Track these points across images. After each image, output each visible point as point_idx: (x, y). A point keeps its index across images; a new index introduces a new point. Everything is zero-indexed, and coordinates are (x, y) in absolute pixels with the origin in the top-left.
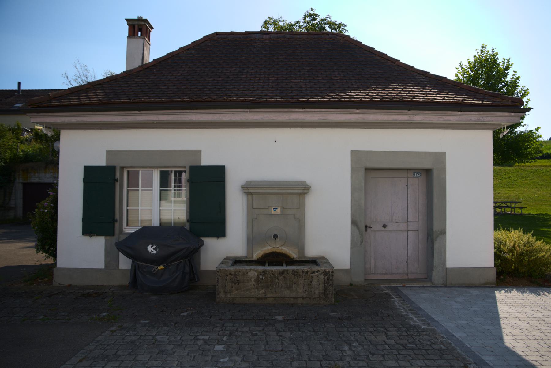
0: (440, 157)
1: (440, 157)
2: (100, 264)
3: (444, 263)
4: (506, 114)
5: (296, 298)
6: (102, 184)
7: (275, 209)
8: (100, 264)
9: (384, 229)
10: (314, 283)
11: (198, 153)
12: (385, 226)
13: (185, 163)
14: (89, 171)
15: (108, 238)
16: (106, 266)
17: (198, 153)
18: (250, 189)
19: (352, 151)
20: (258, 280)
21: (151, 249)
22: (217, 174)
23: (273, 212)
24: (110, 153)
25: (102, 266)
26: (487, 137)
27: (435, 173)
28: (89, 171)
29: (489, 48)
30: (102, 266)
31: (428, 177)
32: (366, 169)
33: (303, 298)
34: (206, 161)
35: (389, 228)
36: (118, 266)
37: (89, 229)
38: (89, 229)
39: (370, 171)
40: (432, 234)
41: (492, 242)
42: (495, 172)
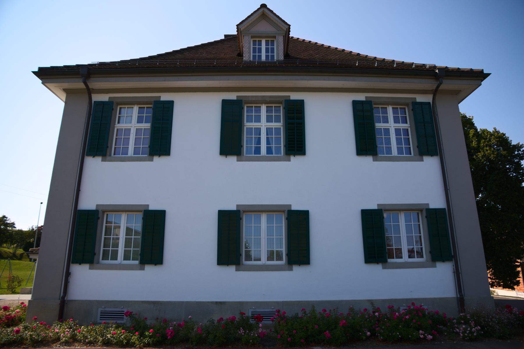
24: (378, 205)
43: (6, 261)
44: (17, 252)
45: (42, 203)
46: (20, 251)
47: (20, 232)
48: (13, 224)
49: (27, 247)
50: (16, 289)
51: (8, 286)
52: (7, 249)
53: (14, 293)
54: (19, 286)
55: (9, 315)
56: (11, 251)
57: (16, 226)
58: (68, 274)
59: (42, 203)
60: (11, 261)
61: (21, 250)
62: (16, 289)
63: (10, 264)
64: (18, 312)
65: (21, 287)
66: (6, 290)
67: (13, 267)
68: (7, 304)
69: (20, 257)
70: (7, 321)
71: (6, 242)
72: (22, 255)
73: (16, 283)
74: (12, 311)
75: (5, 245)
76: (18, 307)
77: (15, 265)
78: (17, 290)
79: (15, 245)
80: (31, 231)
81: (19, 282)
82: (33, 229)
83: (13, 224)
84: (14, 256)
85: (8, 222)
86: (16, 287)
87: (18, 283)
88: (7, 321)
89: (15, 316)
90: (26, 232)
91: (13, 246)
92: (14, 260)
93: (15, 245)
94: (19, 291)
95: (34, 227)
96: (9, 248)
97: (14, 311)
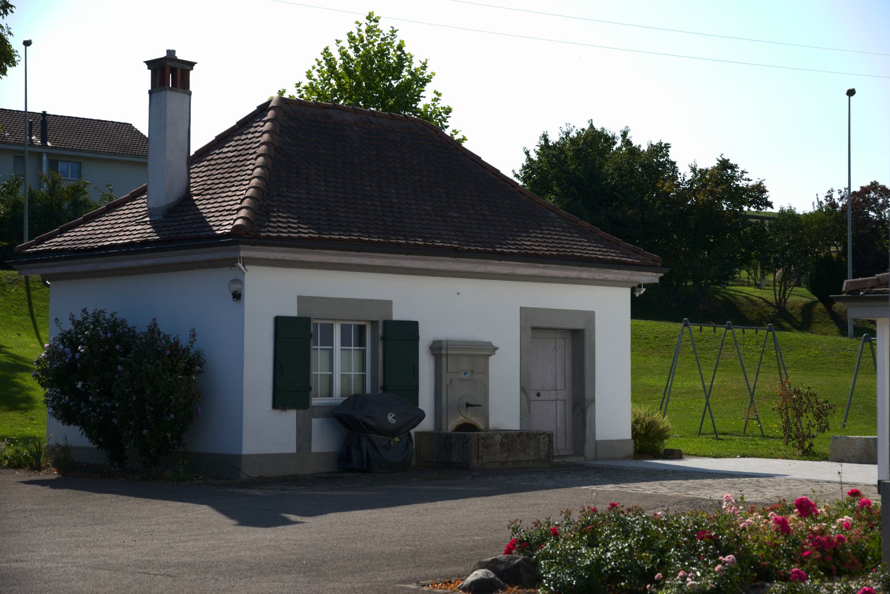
0: (590, 316)
1: (590, 316)
2: (291, 447)
3: (594, 435)
4: (650, 274)
5: (528, 461)
6: (294, 338)
7: (465, 373)
8: (291, 447)
9: (537, 398)
10: (541, 445)
11: (388, 304)
12: (538, 395)
13: (379, 317)
14: (280, 322)
15: (301, 411)
16: (298, 450)
17: (388, 304)
18: (437, 349)
19: (521, 308)
20: (502, 444)
21: (391, 418)
22: (411, 328)
23: (464, 377)
24: (300, 299)
25: (292, 449)
26: (625, 294)
27: (587, 334)
28: (280, 322)
29: (384, 27)
30: (292, 449)
31: (577, 338)
32: (533, 328)
33: (533, 461)
34: (398, 315)
35: (542, 397)
36: (310, 448)
37: (280, 402)
38: (280, 402)
39: (537, 328)
40: (581, 404)
41: (630, 414)
42: (636, 338)
43: (762, 332)
44: (791, 299)
45: (851, 93)
46: (800, 296)
47: (788, 217)
48: (760, 189)
49: (826, 281)
50: (815, 441)
51: (787, 428)
52: (753, 288)
53: (809, 454)
54: (822, 430)
55: (822, 532)
56: (769, 295)
57: (771, 196)
58: (263, 482)
59: (851, 93)
60: (777, 334)
61: (804, 290)
62: (815, 441)
63: (777, 348)
64: (848, 526)
65: (827, 434)
66: (781, 442)
67: (789, 357)
68: (802, 492)
69: (804, 321)
70: (818, 555)
71: (745, 262)
72: (807, 309)
73: (808, 418)
74: (825, 519)
75: (744, 274)
76: (842, 508)
77: (790, 349)
78: (820, 444)
79: (779, 272)
80: (820, 210)
81: (821, 414)
82: (833, 205)
83: (760, 189)
84: (780, 317)
85: (742, 184)
86: (814, 431)
87: (818, 417)
88: (818, 555)
89: (840, 539)
90: (808, 218)
91: (770, 277)
92: (783, 329)
93: (779, 272)
94: (826, 450)
95: (836, 196)
96: (758, 286)
97: (831, 519)
